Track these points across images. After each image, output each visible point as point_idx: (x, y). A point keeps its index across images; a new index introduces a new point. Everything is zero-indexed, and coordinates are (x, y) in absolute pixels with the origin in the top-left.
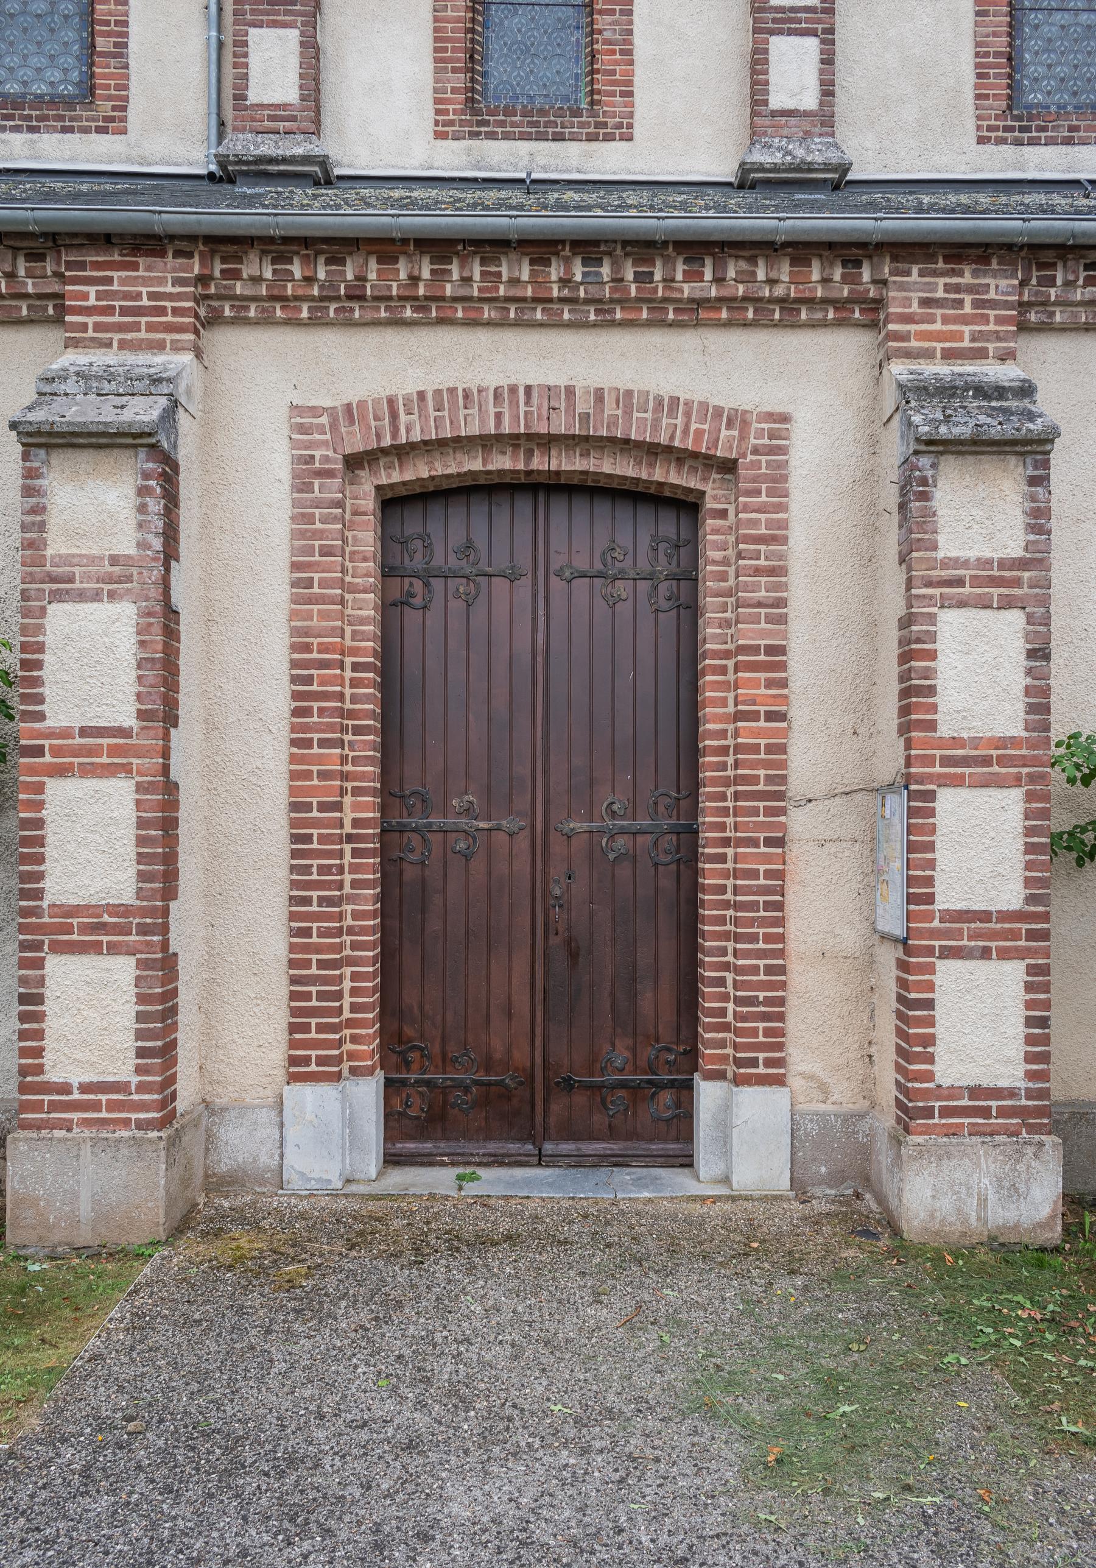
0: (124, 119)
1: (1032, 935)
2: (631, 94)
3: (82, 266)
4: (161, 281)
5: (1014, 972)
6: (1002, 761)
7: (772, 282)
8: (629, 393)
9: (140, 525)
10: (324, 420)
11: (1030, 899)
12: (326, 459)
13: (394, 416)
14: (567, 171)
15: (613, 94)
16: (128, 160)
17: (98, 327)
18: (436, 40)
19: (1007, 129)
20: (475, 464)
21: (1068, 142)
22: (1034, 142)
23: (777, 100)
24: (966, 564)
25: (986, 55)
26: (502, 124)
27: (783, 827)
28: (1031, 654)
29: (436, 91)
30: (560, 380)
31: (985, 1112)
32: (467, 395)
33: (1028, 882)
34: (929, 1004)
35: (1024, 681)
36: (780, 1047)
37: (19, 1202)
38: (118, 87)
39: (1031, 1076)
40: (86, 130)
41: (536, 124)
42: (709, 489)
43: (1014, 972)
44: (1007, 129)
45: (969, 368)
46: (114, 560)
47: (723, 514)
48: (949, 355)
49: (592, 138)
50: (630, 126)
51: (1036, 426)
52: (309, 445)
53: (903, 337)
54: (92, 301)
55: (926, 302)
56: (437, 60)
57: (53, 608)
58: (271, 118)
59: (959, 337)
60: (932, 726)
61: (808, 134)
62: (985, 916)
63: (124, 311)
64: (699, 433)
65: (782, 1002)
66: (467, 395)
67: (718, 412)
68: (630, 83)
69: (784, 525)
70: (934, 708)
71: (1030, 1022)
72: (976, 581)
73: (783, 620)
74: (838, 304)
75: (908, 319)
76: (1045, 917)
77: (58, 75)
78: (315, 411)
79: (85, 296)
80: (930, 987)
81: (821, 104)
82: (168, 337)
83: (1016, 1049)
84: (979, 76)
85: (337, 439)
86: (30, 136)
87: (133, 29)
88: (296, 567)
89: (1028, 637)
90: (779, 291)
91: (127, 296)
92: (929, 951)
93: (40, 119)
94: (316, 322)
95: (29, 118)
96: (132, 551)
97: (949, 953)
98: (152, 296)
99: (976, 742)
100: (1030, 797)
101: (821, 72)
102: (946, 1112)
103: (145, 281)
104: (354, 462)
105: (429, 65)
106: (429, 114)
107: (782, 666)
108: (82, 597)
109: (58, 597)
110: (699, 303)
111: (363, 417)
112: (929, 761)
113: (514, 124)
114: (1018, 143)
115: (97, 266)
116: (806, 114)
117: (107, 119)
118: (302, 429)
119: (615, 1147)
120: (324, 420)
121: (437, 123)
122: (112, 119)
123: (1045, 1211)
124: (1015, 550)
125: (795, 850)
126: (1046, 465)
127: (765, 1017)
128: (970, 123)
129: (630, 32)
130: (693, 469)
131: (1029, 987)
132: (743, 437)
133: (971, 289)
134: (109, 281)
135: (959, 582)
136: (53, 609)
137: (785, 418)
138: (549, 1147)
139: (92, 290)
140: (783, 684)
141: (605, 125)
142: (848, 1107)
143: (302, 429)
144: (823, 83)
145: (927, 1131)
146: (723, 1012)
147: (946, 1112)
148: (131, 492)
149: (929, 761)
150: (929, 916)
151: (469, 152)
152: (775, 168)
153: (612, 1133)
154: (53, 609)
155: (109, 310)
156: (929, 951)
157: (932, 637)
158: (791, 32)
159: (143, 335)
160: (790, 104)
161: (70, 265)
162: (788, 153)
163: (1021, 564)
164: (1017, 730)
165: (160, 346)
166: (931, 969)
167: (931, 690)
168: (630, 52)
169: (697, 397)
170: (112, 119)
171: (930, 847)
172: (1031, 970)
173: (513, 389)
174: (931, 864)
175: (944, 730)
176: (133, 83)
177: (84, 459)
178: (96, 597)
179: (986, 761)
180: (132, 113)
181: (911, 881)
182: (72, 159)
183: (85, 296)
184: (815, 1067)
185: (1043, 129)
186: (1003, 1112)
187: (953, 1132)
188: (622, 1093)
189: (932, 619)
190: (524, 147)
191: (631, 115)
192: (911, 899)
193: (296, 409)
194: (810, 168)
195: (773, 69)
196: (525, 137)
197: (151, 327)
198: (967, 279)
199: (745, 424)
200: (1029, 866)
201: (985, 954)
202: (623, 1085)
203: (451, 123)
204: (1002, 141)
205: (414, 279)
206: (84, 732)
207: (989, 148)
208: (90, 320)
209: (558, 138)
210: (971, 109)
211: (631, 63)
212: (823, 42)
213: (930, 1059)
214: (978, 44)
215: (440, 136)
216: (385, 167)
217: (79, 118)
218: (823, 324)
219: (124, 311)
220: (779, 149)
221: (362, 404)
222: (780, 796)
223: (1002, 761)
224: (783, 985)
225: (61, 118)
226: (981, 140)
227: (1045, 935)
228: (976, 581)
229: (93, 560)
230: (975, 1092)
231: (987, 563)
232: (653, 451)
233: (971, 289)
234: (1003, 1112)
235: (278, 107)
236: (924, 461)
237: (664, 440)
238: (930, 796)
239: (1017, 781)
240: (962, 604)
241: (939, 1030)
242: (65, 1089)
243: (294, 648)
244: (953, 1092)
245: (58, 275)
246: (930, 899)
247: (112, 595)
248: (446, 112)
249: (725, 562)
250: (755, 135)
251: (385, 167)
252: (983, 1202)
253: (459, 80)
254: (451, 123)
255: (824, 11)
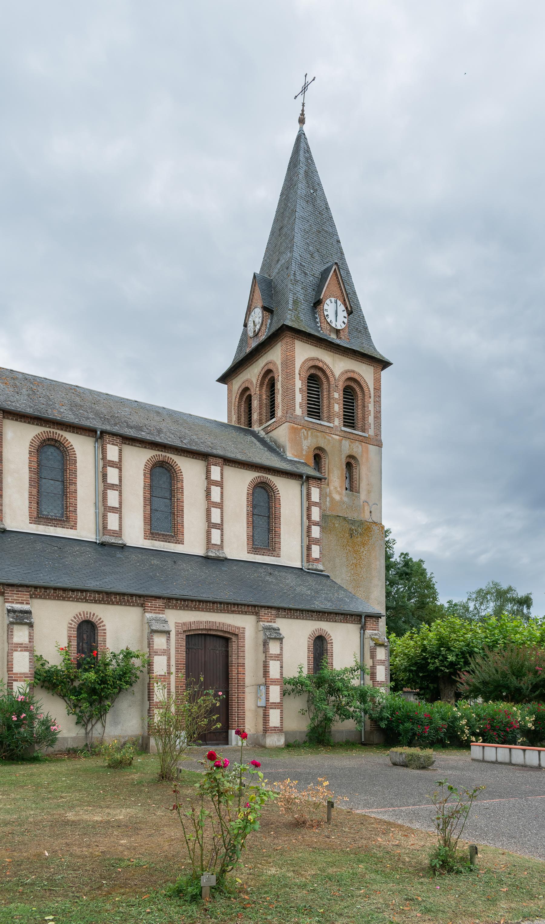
0: (76, 527)
1: (281, 706)
2: (183, 535)
3: (148, 600)
4: (160, 603)
5: (279, 711)
6: (277, 682)
7: (244, 609)
8: (224, 623)
9: (167, 645)
10: (180, 625)
11: (281, 701)
12: (181, 631)
13: (191, 625)
14: (171, 550)
15: (180, 534)
16: (77, 536)
17: (150, 609)
18: (144, 518)
19: (253, 551)
20: (200, 632)
21: (263, 555)
22: (257, 554)
23: (213, 542)
24: (273, 654)
25: (249, 536)
26: (158, 538)
27: (245, 691)
28: (281, 667)
29: (144, 529)
30: (214, 621)
31: (275, 730)
32: (201, 622)
33: (280, 698)
34: (269, 715)
35: (280, 671)
36: (244, 724)
37: (152, 746)
38: (75, 519)
39: (281, 725)
40: (67, 528)
41: (165, 539)
42: (233, 638)
43: (279, 711)
44: (253, 551)
45: (270, 624)
46: (164, 650)
47: (235, 642)
48: (268, 622)
49: (176, 543)
50: (183, 541)
51: (281, 636)
52: (178, 629)
53: (262, 619)
54: (149, 605)
55: (264, 614)
56: (144, 522)
57: (155, 657)
58: (113, 533)
59: (268, 619)
60: (269, 677)
61: (219, 550)
62: (275, 703)
63: (154, 607)
64: (233, 630)
65: (244, 717)
66: (201, 622)
67: (236, 627)
68: (183, 532)
69: (244, 644)
70: (269, 674)
71: (281, 718)
72: (275, 657)
73: (244, 659)
74: (252, 612)
75: (262, 616)
76: (282, 703)
77: (56, 512)
78: (179, 623)
79: (148, 604)
80: (269, 713)
81: (221, 544)
82: (161, 612)
83: (279, 721)
84: (248, 540)
85: (182, 628)
86: (54, 528)
87: (78, 506)
88: (176, 648)
89: (280, 665)
90: (245, 610)
91: (155, 605)
92: (269, 708)
93: (57, 524)
94: (180, 609)
95: (54, 524)
96: (166, 648)
97: (271, 708)
98: (159, 605)
99: (274, 679)
100: (281, 687)
101: (221, 537)
102: (271, 730)
103: (158, 603)
104: (184, 631)
105: (143, 523)
106: (143, 534)
107: (244, 666)
108: (159, 655)
109: (156, 655)
110: (234, 611)
111: (186, 624)
112: (269, 681)
113: (160, 538)
114: (255, 554)
115: (150, 600)
116: (218, 545)
117: (72, 526)
118: (177, 626)
119: (217, 742)
120: (180, 625)
121: (144, 536)
122: (74, 526)
123: (283, 743)
124: (279, 653)
125: (246, 694)
126: (282, 641)
127: (243, 719)
128: (246, 549)
129: (183, 522)
130: (231, 635)
131: (281, 713)
132: (239, 631)
133: (270, 612)
134: (152, 602)
135: (272, 657)
136: (155, 657)
137: (244, 628)
138: (207, 742)
139: (149, 604)
140: (244, 669)
141: (178, 541)
142: (253, 733)
143: (177, 626)
144: (221, 539)
145: (269, 733)
146: (235, 719)
147: (271, 730)
148: (166, 639)
149: (269, 681)
150: (269, 703)
151: (151, 543)
152: (214, 557)
153: (217, 740)
154: (155, 657)
155: (152, 607)
156: (269, 708)
157: (269, 664)
158: (216, 528)
159: (157, 611)
160: (215, 543)
161: (146, 599)
162: (216, 554)
163: (279, 655)
164: (279, 677)
165: (160, 613)
166: (269, 710)
167: (269, 672)
168: (183, 526)
169: (233, 624)
170: (74, 526)
171: (269, 694)
172: (281, 710)
173: (208, 622)
174: (269, 696)
175: (270, 677)
176: (78, 518)
177: (159, 634)
178: (161, 655)
179: (275, 682)
180: (78, 525)
181: (266, 698)
182: (64, 534)
183: (148, 604)
184: (249, 727)
185: (259, 552)
186: (278, 730)
187: (272, 733)
188: (218, 733)
189: (269, 662)
190: (162, 543)
191: (183, 539)
192: (266, 701)
193: (176, 623)
194: (220, 557)
195: (212, 535)
196: (162, 541)
197: (158, 610)
198: (270, 611)
199: (239, 629)
200: (281, 696)
201: (275, 708)
202: (218, 732)
203: (147, 536)
204: (252, 553)
205: (195, 605)
206: (160, 675)
207: (250, 554)
208: (149, 608)
209: (169, 542)
210: (246, 546)
211: (183, 528)
212: (221, 531)
213: (269, 723)
214: (247, 533)
215: (145, 539)
216: (133, 544)
217: (66, 525)
218: (250, 614)
219: (154, 607)
220: (214, 553)
221: (186, 623)
222: (244, 686)
223: (277, 682)
224: (245, 715)
225: (62, 525)
226: (248, 553)
227: (282, 706)
228: (275, 657)
229: (161, 649)
230: (274, 727)
231: (275, 654)
232: (225, 632)
233: (270, 612)
234: (278, 730)
235: (114, 531)
236: (268, 640)
237: (228, 631)
238: (269, 686)
239: (279, 685)
240: (272, 660)
241: (270, 719)
242: (379, 682)
243: (176, 661)
244: (272, 727)
245: (144, 601)
246: (269, 701)
247: (163, 655)
248: (146, 534)
249: (235, 649)
250: (208, 549)
251: (133, 544)
252: (275, 742)
253: (149, 527)
254: (147, 536)
255: (222, 525)
